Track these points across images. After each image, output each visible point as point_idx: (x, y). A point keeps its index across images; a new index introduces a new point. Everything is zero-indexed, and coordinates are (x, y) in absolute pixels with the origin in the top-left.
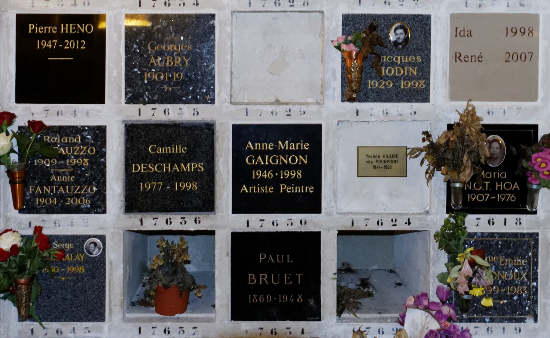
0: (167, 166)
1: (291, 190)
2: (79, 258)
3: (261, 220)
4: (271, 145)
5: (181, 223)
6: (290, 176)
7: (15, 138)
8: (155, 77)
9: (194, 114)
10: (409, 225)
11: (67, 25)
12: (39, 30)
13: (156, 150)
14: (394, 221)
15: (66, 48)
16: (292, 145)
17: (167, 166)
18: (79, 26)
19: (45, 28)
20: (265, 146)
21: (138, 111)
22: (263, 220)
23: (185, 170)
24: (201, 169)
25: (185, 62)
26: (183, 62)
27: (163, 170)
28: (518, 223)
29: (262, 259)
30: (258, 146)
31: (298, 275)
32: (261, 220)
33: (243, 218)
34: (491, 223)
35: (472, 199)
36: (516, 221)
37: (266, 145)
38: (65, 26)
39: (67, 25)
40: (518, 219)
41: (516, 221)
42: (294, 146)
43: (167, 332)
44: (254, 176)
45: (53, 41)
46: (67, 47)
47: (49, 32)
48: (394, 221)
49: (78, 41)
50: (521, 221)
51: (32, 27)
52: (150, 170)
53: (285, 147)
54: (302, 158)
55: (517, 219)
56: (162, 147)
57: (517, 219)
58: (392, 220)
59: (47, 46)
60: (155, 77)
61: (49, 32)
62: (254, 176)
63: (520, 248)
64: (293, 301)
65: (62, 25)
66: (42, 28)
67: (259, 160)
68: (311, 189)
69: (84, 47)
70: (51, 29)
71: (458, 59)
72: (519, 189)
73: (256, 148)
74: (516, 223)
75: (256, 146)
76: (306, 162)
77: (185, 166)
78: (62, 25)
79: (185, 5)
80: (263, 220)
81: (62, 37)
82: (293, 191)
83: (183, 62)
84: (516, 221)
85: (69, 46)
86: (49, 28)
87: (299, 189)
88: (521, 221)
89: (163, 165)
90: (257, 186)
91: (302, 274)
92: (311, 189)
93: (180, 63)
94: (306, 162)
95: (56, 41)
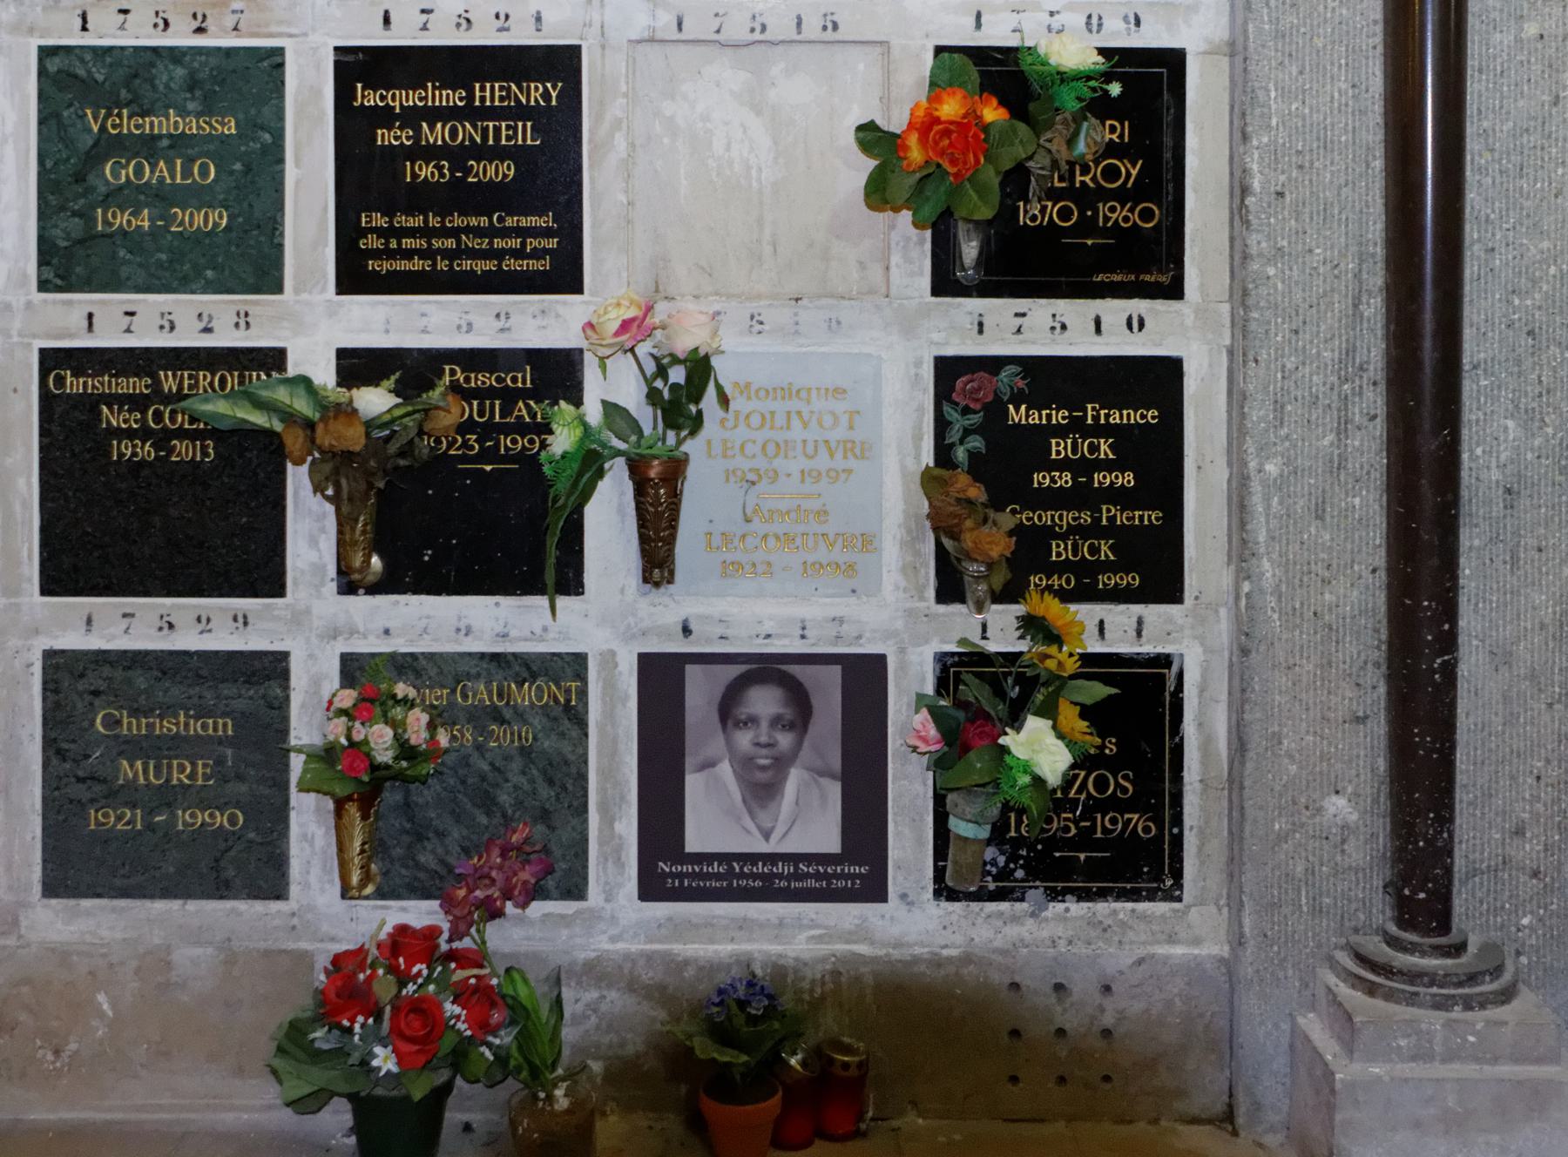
1: (426, 98)
2: (524, 412)
5: (507, 17)
6: (1112, 483)
11: (488, 85)
13: (504, 221)
18: (514, 87)
19: (1137, 513)
20: (85, 383)
23: (431, 141)
28: (242, 324)
30: (1129, 415)
36: (235, 319)
38: (483, 89)
39: (488, 85)
40: (242, 315)
44: (179, 168)
47: (1146, 523)
48: (204, 620)
51: (1109, 511)
55: (238, 314)
56: (512, 216)
57: (238, 314)
58: (497, 16)
61: (1146, 523)
65: (477, 85)
68: (1152, 517)
70: (1150, 516)
71: (849, 454)
74: (237, 325)
78: (477, 85)
82: (430, 104)
84: (235, 319)
85: (477, 175)
86: (1146, 513)
90: (111, 376)
92: (1152, 517)
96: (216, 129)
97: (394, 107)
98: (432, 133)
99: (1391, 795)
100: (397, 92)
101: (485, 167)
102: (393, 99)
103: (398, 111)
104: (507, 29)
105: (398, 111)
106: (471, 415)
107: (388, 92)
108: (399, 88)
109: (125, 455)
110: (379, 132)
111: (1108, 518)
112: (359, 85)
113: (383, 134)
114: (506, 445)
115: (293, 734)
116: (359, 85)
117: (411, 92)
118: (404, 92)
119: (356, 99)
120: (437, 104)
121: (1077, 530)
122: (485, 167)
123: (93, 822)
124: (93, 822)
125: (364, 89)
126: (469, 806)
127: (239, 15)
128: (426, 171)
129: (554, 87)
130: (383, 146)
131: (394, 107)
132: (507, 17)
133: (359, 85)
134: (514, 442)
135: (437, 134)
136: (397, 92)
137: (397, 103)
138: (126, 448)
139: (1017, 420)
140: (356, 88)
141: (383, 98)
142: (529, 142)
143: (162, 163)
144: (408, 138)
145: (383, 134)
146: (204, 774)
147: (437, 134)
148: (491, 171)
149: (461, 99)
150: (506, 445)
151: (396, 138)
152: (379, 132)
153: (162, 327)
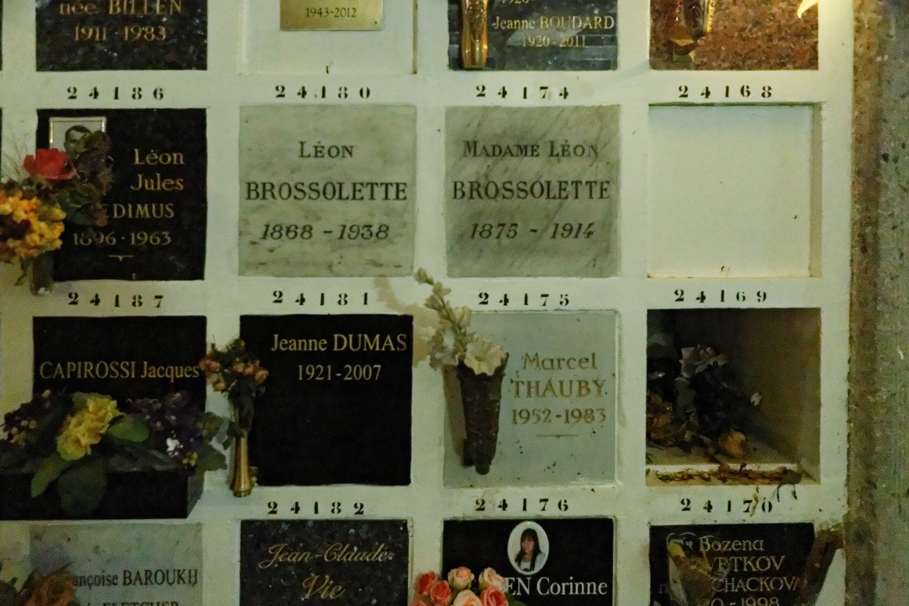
4: (737, 543)
7: (658, 601)
8: (353, 369)
9: (561, 303)
10: (565, 97)
12: (295, 345)
15: (346, 378)
16: (293, 342)
21: (363, 298)
23: (371, 348)
24: (179, 187)
33: (62, 80)
35: (309, 376)
37: (750, 543)
40: (137, 298)
42: (295, 344)
43: (158, 96)
44: (301, 375)
45: (376, 366)
46: (349, 377)
52: (400, 348)
53: (375, 346)
54: (776, 565)
57: (764, 88)
60: (353, 369)
62: (301, 375)
67: (740, 585)
69: (321, 377)
75: (69, 366)
79: (569, 509)
81: (340, 360)
84: (762, 91)
85: (351, 375)
87: (177, 374)
95: (379, 366)
96: (124, 374)
98: (372, 343)
99: (820, 341)
101: (358, 368)
103: (172, 381)
105: (172, 381)
106: (752, 543)
107: (165, 368)
108: (174, 365)
109: (309, 376)
111: (71, 373)
112: (276, 336)
118: (177, 368)
119: (273, 345)
120: (305, 349)
121: (329, 590)
122: (358, 368)
125: (149, 366)
126: (592, 60)
127: (159, 300)
128: (363, 372)
133: (146, 363)
137: (172, 375)
138: (310, 370)
139: (371, 348)
141: (162, 372)
143: (388, 337)
148: (362, 372)
149: (323, 346)
152: (336, 336)
153: (339, 302)
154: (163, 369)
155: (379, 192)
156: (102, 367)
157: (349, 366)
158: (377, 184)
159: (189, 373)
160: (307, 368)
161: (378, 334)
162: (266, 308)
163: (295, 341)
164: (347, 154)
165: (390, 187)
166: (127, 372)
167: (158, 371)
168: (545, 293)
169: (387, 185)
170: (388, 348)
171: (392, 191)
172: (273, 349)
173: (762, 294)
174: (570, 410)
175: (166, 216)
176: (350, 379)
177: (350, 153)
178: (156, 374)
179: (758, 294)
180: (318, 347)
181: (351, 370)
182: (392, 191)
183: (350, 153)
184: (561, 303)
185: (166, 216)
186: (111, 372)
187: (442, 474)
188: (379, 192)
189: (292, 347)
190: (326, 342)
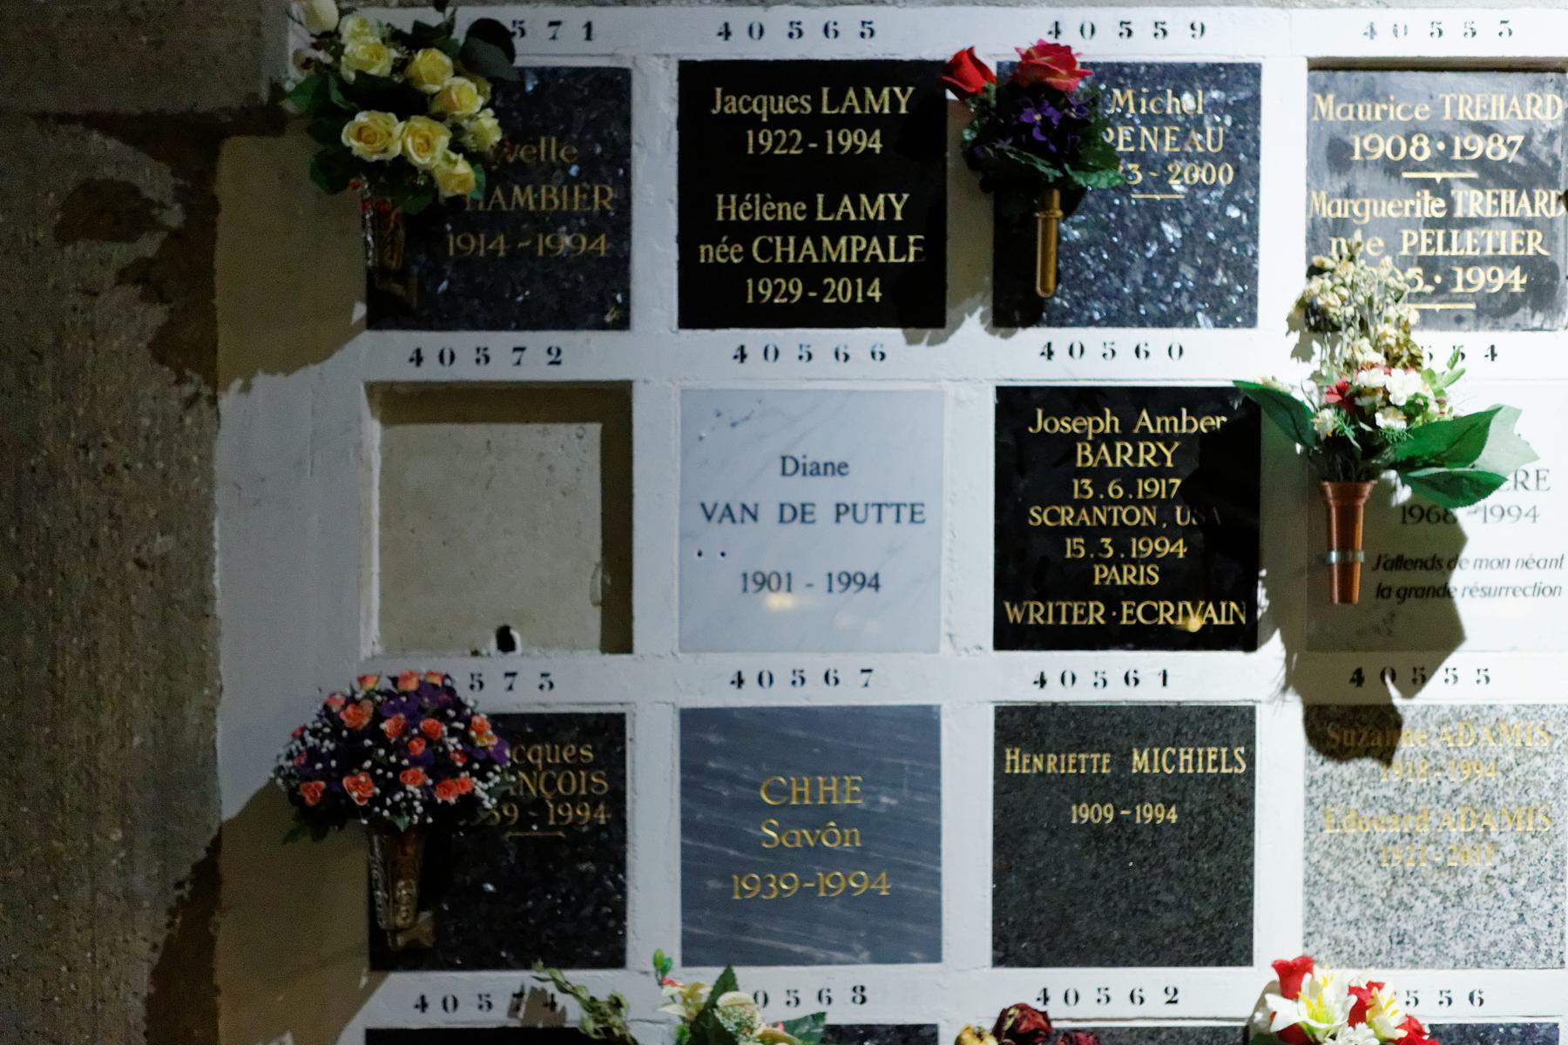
0: (785, 243)
3: (863, 671)
14: (812, 513)
15: (826, 300)
17: (785, 243)
22: (869, 671)
25: (1165, 458)
26: (1160, 457)
27: (775, 257)
29: (1102, 617)
31: (1444, 100)
32: (863, 671)
34: (832, 681)
38: (727, 201)
41: (853, 994)
42: (733, 103)
48: (554, 351)
49: (859, 281)
50: (865, 994)
58: (549, 351)
59: (870, 146)
63: (458, 201)
64: (606, 251)
66: (726, 250)
72: (921, 237)
73: (1167, 430)
76: (1145, 414)
77: (834, 247)
80: (869, 671)
83: (1160, 457)
85: (835, 294)
88: (865, 994)
89: (775, 241)
91: (1031, 430)
93: (1102, 617)
94: (1145, 414)
97: (760, 116)
98: (834, 249)
100: (765, 98)
102: (760, 106)
104: (558, 363)
105: (765, 119)
107: (753, 98)
108: (768, 94)
110: (703, 248)
112: (719, 90)
113: (707, 251)
114: (1144, 490)
115: (1485, 453)
116: (719, 90)
117: (781, 98)
118: (772, 99)
123: (552, 816)
124: (552, 816)
125: (724, 94)
129: (899, 199)
130: (706, 264)
131: (760, 116)
132: (559, 352)
134: (1152, 485)
135: (785, 249)
136: (765, 98)
139: (834, 258)
140: (715, 92)
142: (892, 259)
144: (737, 255)
145: (707, 251)
146: (1079, 615)
147: (785, 249)
149: (800, 213)
150: (1144, 490)
151: (723, 255)
154: (749, 99)
155: (889, 514)
156: (1396, 153)
157: (831, 280)
158: (887, 505)
159: (793, 106)
160: (761, 136)
161: (502, 258)
162: (1029, 694)
163: (734, 99)
164: (747, 517)
165: (902, 508)
166: (1064, 424)
167: (741, 102)
168: (866, 667)
169: (898, 506)
170: (808, 258)
171: (905, 513)
172: (714, 112)
173: (1198, 26)
174: (1442, 522)
175: (1148, 582)
176: (834, 300)
177: (755, 518)
178: (737, 108)
179: (1192, 27)
180: (792, 216)
181: (833, 287)
182: (905, 513)
183: (755, 518)
184: (472, 687)
185: (1148, 582)
186: (1040, 514)
187: (789, 338)
188: (889, 514)
189: (730, 108)
190: (804, 207)
